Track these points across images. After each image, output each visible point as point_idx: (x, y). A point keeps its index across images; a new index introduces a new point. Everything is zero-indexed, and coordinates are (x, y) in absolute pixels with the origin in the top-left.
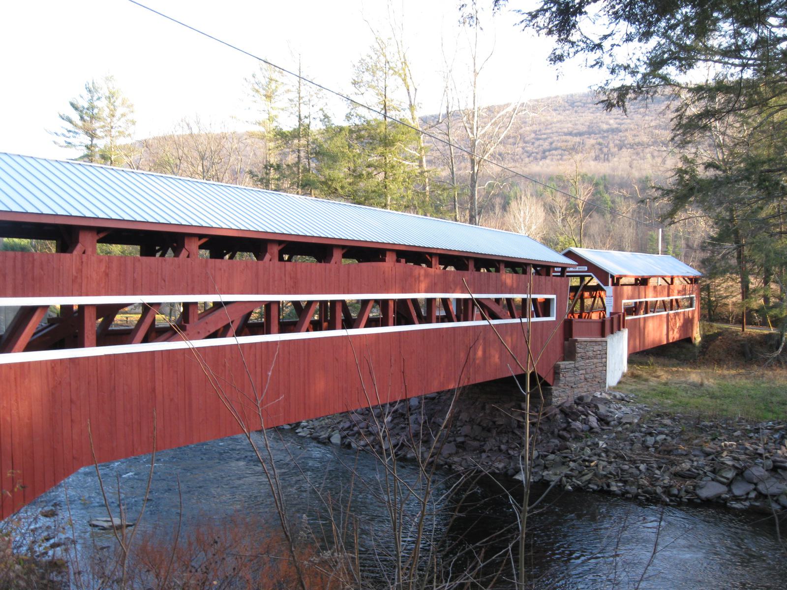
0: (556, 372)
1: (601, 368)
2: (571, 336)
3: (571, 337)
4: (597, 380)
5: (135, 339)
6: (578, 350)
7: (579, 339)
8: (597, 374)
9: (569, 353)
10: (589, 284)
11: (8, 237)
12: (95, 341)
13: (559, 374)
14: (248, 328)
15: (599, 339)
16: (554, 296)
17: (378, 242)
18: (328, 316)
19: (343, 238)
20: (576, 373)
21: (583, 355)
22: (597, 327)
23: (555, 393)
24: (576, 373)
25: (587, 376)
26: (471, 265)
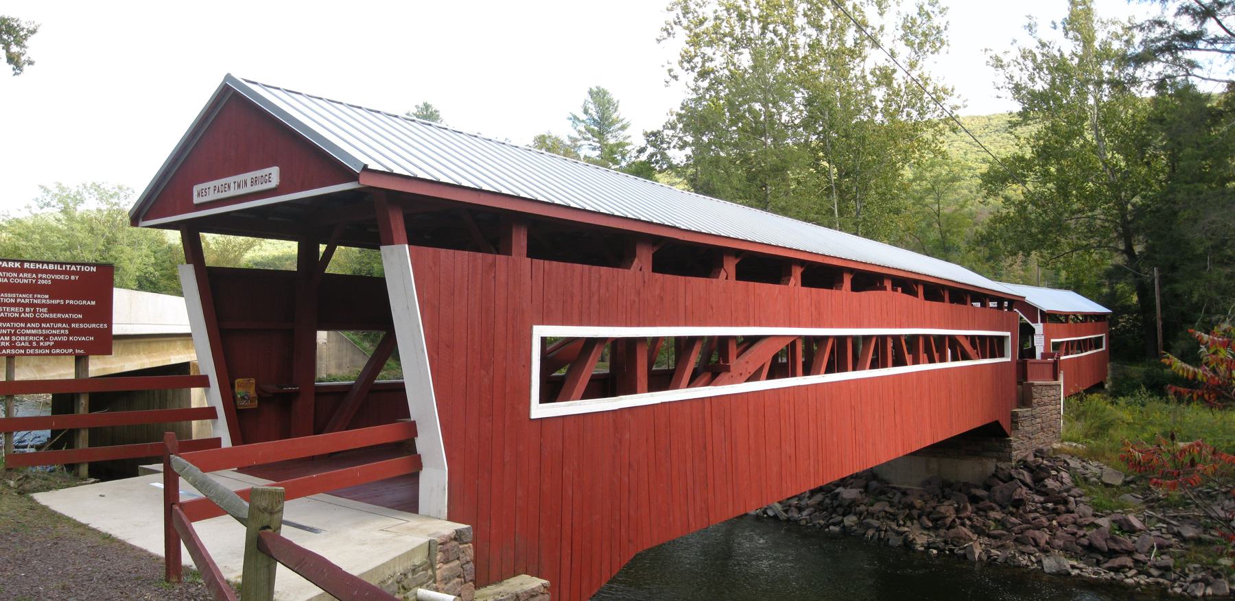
8: (1052, 423)
9: (1025, 399)
15: (1054, 382)
16: (1008, 334)
18: (841, 354)
22: (1048, 370)
23: (1014, 445)
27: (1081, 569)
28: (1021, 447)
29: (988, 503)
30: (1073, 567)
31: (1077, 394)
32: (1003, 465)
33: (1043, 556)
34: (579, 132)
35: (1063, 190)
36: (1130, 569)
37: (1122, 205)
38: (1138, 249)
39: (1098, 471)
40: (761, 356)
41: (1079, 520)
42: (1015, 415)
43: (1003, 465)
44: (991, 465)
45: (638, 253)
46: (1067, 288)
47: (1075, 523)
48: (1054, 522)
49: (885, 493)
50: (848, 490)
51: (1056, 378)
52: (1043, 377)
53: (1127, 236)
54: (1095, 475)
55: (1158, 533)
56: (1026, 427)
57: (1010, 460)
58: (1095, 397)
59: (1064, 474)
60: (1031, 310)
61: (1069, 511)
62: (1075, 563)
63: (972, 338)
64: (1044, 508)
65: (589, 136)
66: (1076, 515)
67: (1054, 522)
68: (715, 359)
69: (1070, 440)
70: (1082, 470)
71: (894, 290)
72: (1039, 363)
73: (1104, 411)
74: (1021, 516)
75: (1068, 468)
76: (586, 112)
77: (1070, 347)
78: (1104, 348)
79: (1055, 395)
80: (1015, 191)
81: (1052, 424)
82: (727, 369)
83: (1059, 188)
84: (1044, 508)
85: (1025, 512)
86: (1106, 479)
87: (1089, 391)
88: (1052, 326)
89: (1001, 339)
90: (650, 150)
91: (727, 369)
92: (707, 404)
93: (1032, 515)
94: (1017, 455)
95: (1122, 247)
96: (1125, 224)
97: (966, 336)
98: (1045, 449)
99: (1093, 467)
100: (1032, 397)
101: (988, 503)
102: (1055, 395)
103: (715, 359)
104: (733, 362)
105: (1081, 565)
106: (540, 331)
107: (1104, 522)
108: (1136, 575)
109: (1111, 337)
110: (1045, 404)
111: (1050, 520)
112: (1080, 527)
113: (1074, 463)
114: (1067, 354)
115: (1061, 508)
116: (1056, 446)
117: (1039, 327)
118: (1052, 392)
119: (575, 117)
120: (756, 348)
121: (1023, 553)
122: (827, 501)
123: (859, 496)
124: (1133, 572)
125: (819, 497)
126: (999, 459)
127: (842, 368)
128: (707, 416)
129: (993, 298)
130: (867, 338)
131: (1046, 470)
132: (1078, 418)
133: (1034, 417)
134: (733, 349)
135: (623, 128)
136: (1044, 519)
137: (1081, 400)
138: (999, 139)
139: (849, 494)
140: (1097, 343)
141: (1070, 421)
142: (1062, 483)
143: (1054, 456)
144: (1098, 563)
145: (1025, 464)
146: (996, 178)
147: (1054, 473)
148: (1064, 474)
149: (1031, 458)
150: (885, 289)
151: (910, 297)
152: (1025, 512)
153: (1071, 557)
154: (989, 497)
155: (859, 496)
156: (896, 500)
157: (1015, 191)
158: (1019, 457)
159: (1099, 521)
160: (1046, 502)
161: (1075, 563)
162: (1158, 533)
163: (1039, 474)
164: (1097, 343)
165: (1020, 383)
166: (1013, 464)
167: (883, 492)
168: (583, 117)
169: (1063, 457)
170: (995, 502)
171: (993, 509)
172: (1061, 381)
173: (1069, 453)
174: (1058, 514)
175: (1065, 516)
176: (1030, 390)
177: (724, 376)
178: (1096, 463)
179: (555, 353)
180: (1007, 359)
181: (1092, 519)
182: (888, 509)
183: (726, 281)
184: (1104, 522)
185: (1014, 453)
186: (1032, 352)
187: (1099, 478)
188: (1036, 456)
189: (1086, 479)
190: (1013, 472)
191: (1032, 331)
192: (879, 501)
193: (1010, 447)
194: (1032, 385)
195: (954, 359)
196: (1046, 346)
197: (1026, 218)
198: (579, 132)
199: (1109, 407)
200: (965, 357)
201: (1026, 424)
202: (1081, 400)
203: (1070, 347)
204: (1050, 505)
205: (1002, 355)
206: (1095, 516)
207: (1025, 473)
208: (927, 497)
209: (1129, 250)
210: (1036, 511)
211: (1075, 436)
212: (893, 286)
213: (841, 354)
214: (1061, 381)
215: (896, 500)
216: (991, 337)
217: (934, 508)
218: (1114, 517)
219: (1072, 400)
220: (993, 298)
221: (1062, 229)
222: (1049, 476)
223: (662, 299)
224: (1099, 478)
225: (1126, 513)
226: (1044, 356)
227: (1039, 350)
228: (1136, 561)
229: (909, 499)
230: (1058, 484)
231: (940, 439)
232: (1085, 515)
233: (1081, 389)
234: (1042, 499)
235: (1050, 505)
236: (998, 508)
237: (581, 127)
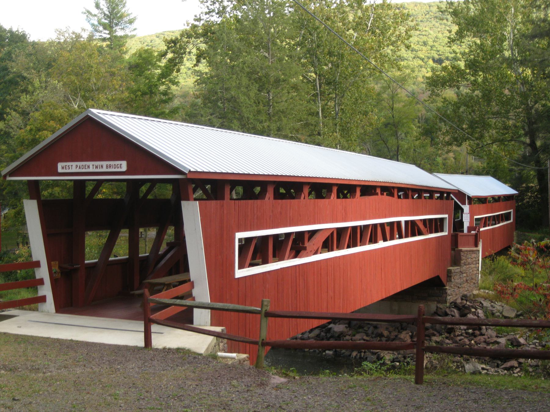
0: (449, 274)
1: (475, 272)
2: (457, 247)
3: (457, 247)
4: (473, 281)
5: (378, 239)
6: (463, 258)
7: (463, 249)
8: (474, 277)
9: (456, 260)
10: (150, 197)
11: (116, 199)
12: (186, 273)
13: (451, 277)
14: (327, 246)
15: (475, 249)
16: (446, 216)
17: (234, 174)
18: (355, 236)
19: (235, 172)
20: (461, 276)
21: (465, 261)
22: (472, 240)
23: (449, 292)
24: (461, 276)
25: (468, 278)
26: (378, 191)
27: (487, 370)
28: (453, 294)
29: (431, 331)
30: (483, 369)
31: (490, 256)
32: (441, 306)
33: (464, 363)
34: (93, 25)
35: (487, 96)
36: (516, 368)
37: (528, 109)
38: (538, 143)
39: (500, 308)
40: (319, 240)
41: (488, 340)
42: (449, 272)
43: (441, 306)
44: (433, 306)
45: (268, 189)
46: (487, 174)
47: (485, 342)
48: (473, 342)
49: (363, 328)
50: (337, 325)
51: (476, 245)
52: (468, 245)
53: (532, 134)
54: (499, 311)
55: (533, 346)
56: (456, 279)
57: (446, 302)
58: (502, 259)
59: (480, 311)
60: (460, 195)
61: (482, 335)
62: (484, 366)
63: (424, 221)
64: (467, 333)
65: (101, 28)
66: (486, 337)
67: (473, 342)
68: (298, 244)
69: (485, 288)
70: (491, 308)
71: (382, 194)
72: (466, 235)
73: (506, 268)
74: (452, 339)
75: (482, 307)
76: (97, 6)
77: (486, 222)
78: (512, 221)
79: (477, 256)
80: (450, 93)
81: (474, 278)
82: (305, 248)
83: (484, 96)
84: (467, 333)
85: (455, 336)
86: (505, 314)
87: (499, 253)
88: (476, 206)
89: (442, 220)
90: (170, 55)
91: (305, 248)
92: (297, 268)
93: (459, 338)
94: (450, 299)
95: (528, 141)
96: (531, 123)
97: (421, 220)
98: (468, 295)
99: (498, 306)
100: (460, 259)
101: (431, 331)
102: (477, 256)
103: (298, 244)
104: (307, 244)
105: (488, 368)
106: (239, 235)
107: (503, 341)
108: (519, 372)
109: (517, 211)
110: (469, 264)
111: (470, 341)
112: (488, 344)
113: (486, 304)
114: (484, 227)
115: (477, 332)
116: (475, 292)
117: (466, 208)
118: (474, 255)
119: (88, 12)
120: (317, 236)
121: (454, 362)
122: (323, 334)
123: (345, 330)
124: (518, 370)
125: (317, 332)
126: (439, 302)
127: (355, 245)
128: (298, 274)
129: (437, 192)
130: (366, 227)
131: (468, 308)
132: (490, 274)
133: (462, 273)
134: (307, 236)
135: (131, 22)
136: (466, 340)
137: (493, 260)
138: (437, 25)
139: (338, 328)
140: (506, 217)
141: (485, 275)
142: (478, 316)
143: (474, 299)
144: (498, 366)
145: (455, 305)
146: (435, 83)
147: (473, 310)
148: (480, 311)
149: (459, 301)
150: (377, 194)
151: (391, 198)
152: (455, 336)
153: (482, 363)
154: (432, 328)
155: (345, 330)
156: (370, 332)
157: (450, 93)
158: (451, 300)
159: (499, 340)
160: (468, 329)
161: (484, 366)
162: (533, 346)
163: (463, 310)
164: (506, 217)
165: (453, 249)
166: (448, 305)
167: (361, 327)
168: (95, 11)
169: (479, 300)
170: (436, 330)
171: (434, 335)
172: (480, 248)
173: (483, 297)
174: (475, 336)
175: (479, 337)
176: (460, 255)
177: (302, 252)
178: (500, 304)
179: (246, 243)
180: (445, 233)
181: (495, 339)
182: (365, 337)
183: (306, 201)
184: (503, 341)
185: (448, 298)
186: (461, 223)
187: (501, 313)
188: (462, 299)
189: (493, 314)
190: (448, 310)
191: (462, 210)
192: (358, 333)
193: (446, 293)
194: (461, 251)
195: (399, 223)
196: (471, 222)
197: (459, 117)
198: (93, 25)
199: (510, 265)
200: (420, 234)
201: (457, 277)
202: (493, 260)
203: (486, 222)
204: (470, 331)
205: (442, 231)
206: (497, 337)
207: (455, 311)
208: (391, 329)
209: (532, 144)
210: (461, 335)
211: (488, 286)
212: (381, 191)
213: (355, 236)
214: (480, 248)
215: (370, 332)
216: (436, 219)
217: (396, 336)
218: (508, 337)
219: (487, 261)
220: (437, 192)
221: (486, 126)
222: (470, 312)
223: (281, 213)
224: (501, 313)
225: (516, 334)
226: (470, 229)
227: (466, 224)
228: (520, 363)
229: (380, 331)
230: (475, 317)
231: (405, 288)
232: (491, 337)
233: (493, 252)
234: (465, 327)
235: (470, 331)
236: (438, 335)
237: (95, 21)
